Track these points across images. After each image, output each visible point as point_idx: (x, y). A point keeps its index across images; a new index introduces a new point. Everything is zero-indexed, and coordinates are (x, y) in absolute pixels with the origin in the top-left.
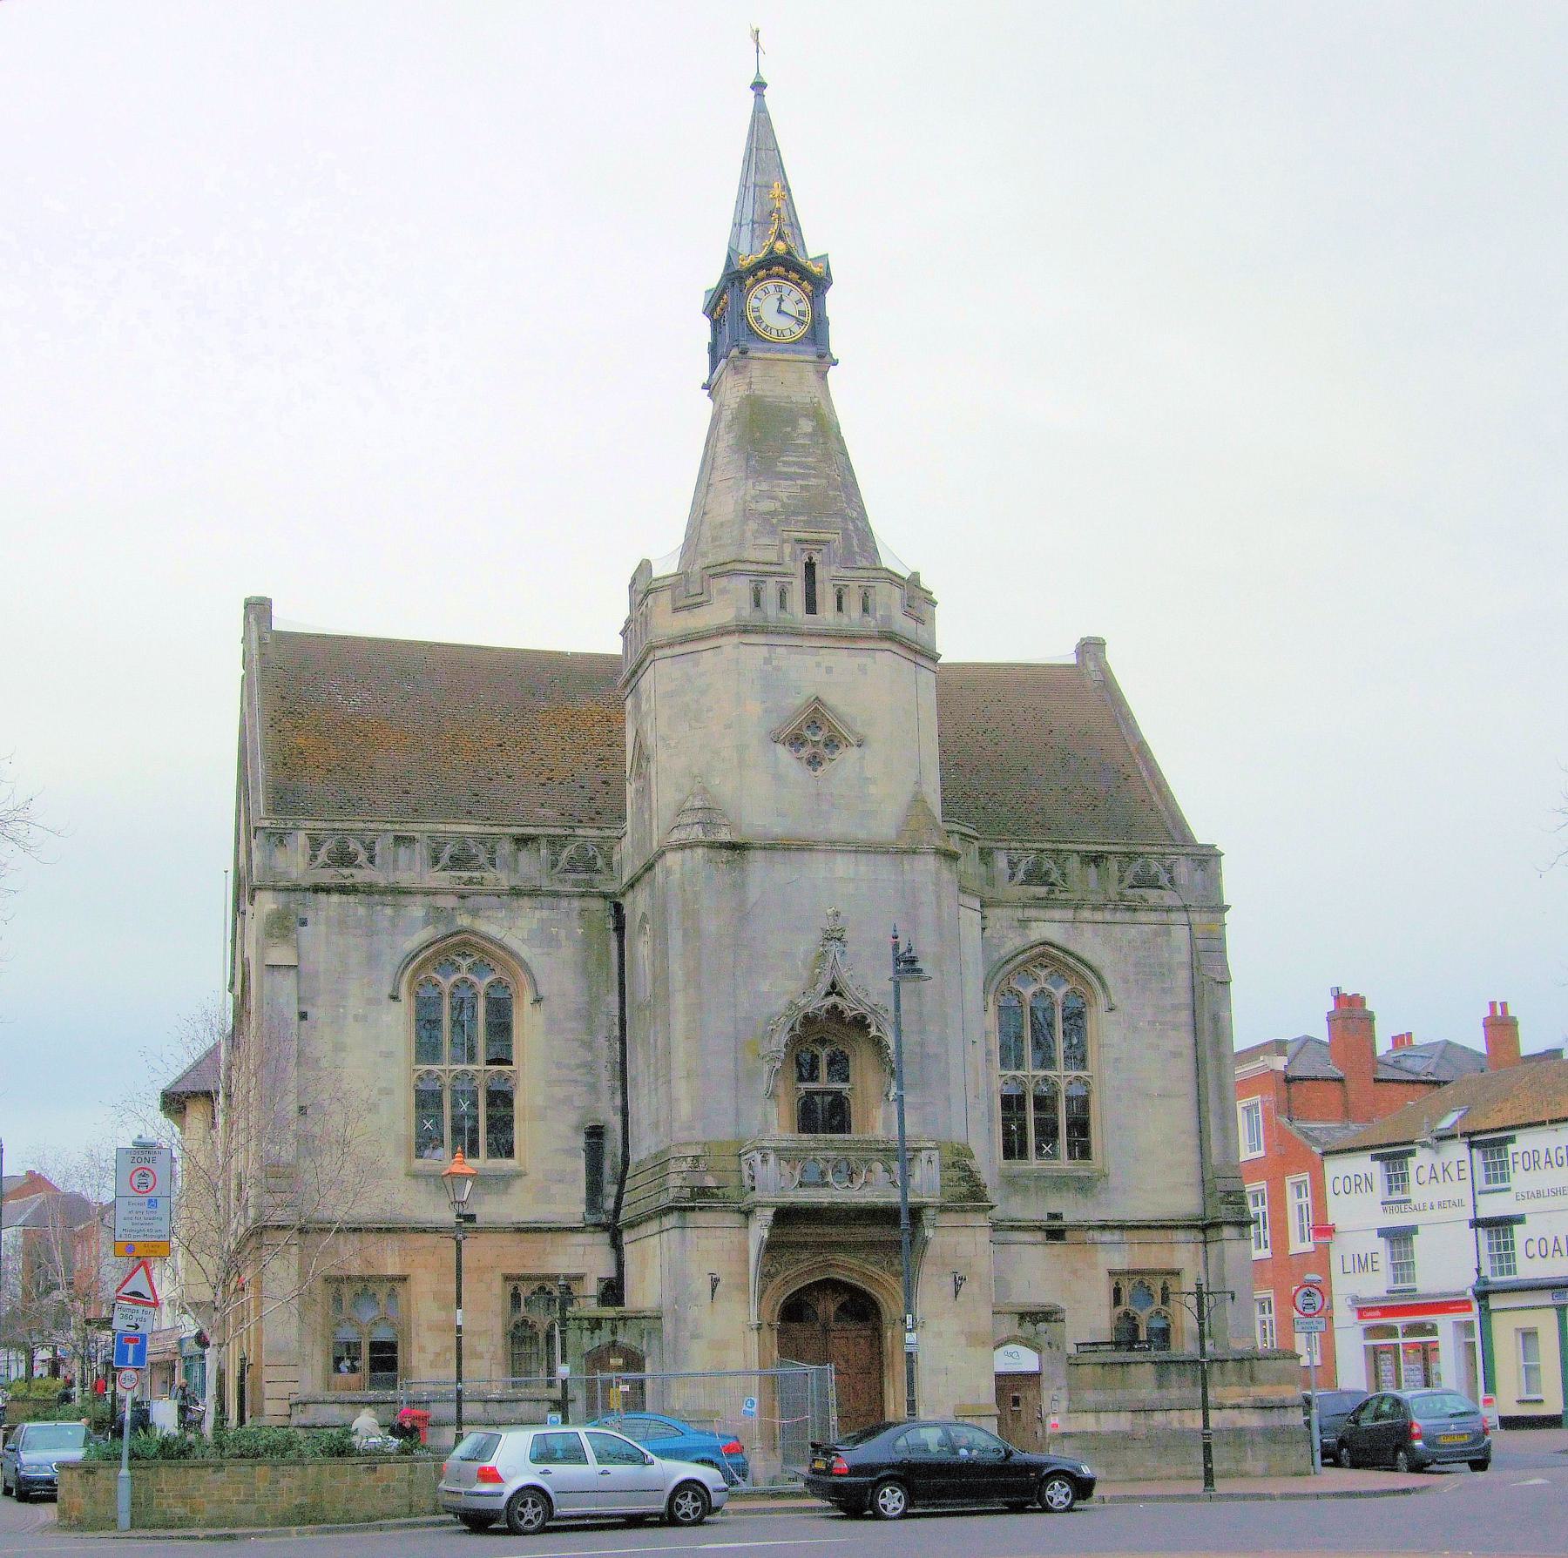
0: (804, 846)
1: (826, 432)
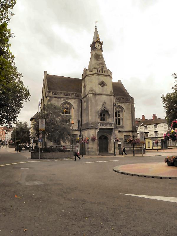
0: (101, 94)
1: (102, 57)
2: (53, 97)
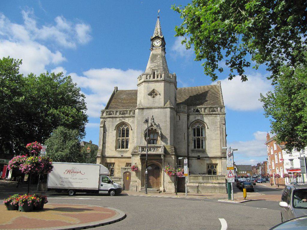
0: (151, 108)
2: (107, 118)
